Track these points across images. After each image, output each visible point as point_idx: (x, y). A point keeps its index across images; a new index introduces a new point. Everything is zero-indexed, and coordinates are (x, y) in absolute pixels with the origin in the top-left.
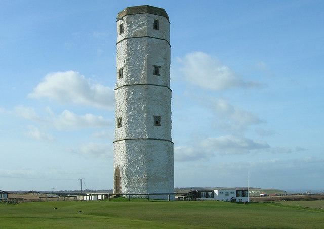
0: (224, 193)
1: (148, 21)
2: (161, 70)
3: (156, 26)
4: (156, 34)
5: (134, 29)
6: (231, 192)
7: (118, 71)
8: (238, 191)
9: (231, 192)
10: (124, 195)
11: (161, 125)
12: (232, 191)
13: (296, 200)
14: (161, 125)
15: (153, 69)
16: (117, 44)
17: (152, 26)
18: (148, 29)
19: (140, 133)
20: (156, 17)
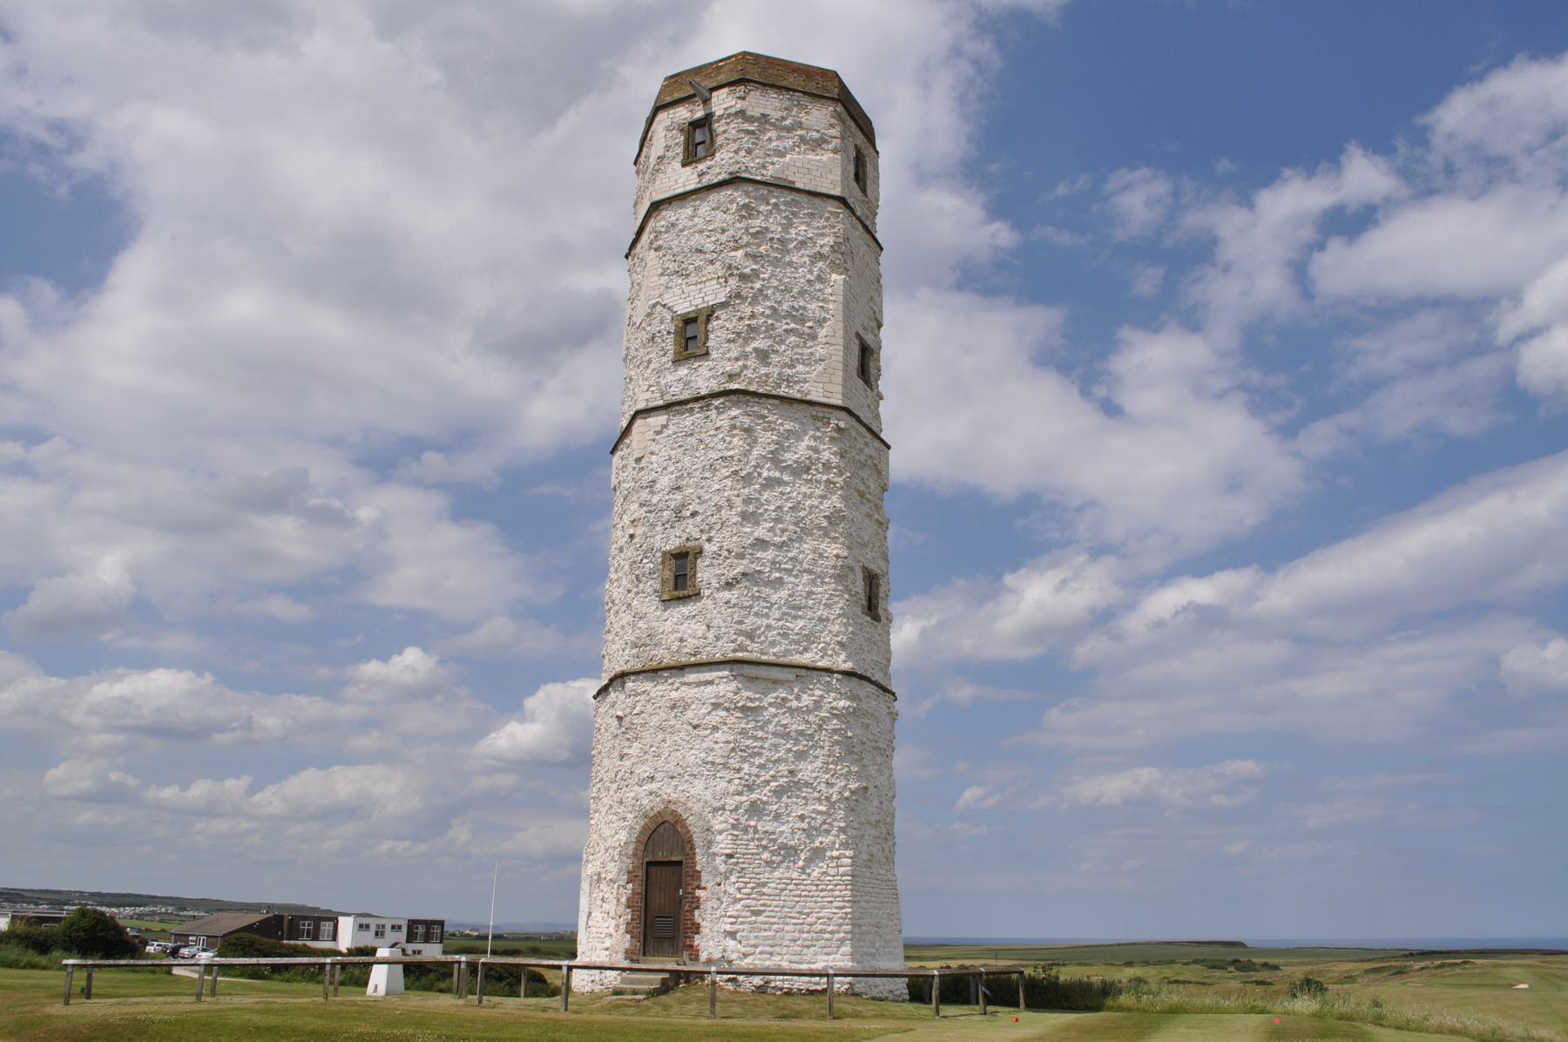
0: (373, 929)
6: (393, 927)
9: (393, 927)
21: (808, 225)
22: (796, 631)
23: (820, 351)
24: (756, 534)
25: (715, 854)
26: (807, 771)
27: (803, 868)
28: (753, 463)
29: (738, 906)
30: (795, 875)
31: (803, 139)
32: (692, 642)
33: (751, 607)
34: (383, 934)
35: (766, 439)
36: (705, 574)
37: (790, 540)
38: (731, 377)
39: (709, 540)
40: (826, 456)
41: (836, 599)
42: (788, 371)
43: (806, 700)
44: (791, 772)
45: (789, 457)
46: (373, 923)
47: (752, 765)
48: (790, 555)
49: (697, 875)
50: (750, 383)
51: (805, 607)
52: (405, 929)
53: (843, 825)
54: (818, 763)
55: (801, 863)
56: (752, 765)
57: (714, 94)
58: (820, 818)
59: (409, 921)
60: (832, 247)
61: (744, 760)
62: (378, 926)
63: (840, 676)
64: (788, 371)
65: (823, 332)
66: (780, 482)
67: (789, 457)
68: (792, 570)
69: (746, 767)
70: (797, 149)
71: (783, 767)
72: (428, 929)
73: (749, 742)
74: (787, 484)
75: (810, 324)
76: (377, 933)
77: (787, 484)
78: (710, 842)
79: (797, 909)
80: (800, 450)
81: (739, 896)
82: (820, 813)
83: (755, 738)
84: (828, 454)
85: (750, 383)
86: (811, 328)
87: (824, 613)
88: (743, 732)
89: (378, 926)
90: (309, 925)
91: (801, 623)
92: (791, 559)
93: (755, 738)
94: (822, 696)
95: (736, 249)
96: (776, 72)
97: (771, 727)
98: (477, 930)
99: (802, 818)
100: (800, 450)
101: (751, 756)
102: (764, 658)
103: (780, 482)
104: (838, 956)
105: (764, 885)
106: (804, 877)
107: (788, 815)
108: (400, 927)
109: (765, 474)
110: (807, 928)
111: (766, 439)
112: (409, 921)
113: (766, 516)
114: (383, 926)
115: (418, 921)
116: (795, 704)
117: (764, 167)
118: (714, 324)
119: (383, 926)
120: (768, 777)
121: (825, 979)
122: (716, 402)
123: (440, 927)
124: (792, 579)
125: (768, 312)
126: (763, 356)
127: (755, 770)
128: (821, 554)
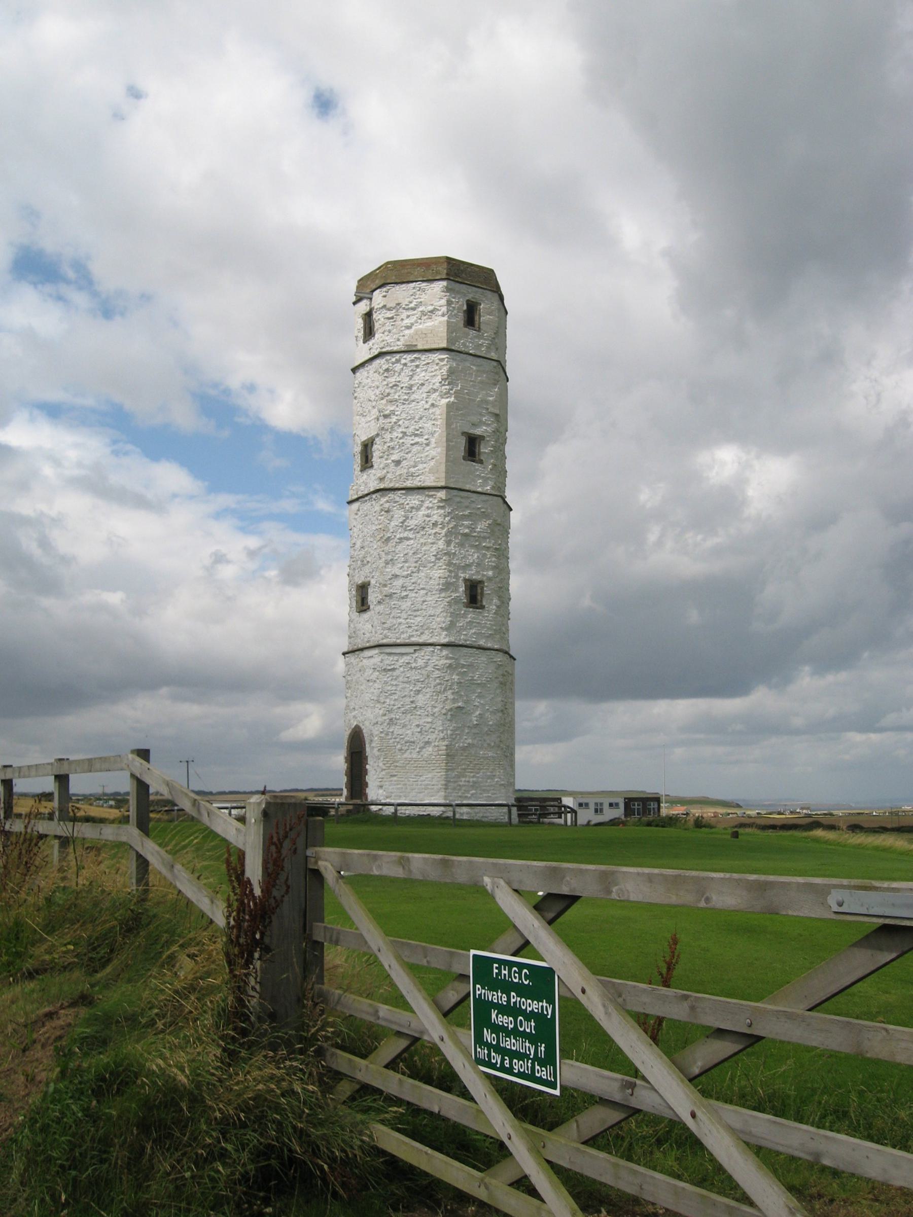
0: (592, 807)
1: (449, 303)
2: (485, 449)
3: (471, 316)
4: (469, 341)
5: (167, 987)
6: (611, 805)
7: (358, 449)
8: (629, 802)
9: (611, 805)
10: (374, 808)
11: (482, 607)
12: (613, 800)
13: (764, 828)
14: (482, 607)
15: (462, 442)
16: (354, 370)
17: (460, 318)
18: (450, 328)
19: (423, 628)
20: (472, 293)
21: (426, 371)
22: (416, 624)
23: (433, 453)
24: (393, 572)
25: (373, 747)
26: (421, 700)
27: (418, 752)
28: (391, 531)
29: (384, 773)
30: (414, 756)
31: (423, 313)
32: (368, 635)
33: (390, 614)
34: (601, 810)
35: (398, 514)
36: (372, 597)
37: (412, 572)
38: (382, 479)
39: (373, 577)
40: (435, 518)
41: (440, 603)
42: (412, 470)
43: (420, 663)
44: (412, 702)
45: (412, 523)
46: (592, 802)
47: (391, 699)
48: (412, 581)
49: (366, 758)
50: (391, 482)
51: (421, 610)
52: (622, 806)
53: (441, 728)
54: (428, 696)
55: (418, 750)
56: (391, 699)
57: (375, 293)
58: (428, 725)
59: (625, 799)
60: (440, 383)
61: (386, 697)
62: (596, 804)
63: (439, 647)
64: (412, 470)
65: (433, 440)
66: (408, 539)
67: (412, 523)
68: (413, 590)
69: (388, 700)
70: (419, 321)
71: (408, 700)
72: (644, 806)
73: (389, 688)
74: (411, 539)
75: (426, 437)
76: (596, 811)
77: (411, 539)
78: (371, 741)
79: (415, 773)
80: (418, 518)
81: (384, 768)
82: (428, 723)
83: (392, 685)
84: (437, 515)
85: (391, 482)
86: (427, 439)
87: (431, 612)
88: (386, 683)
89: (596, 804)
90: (638, 805)
91: (419, 619)
92: (413, 583)
93: (392, 685)
94: (429, 660)
95: (382, 399)
96: (406, 271)
97: (401, 679)
98: (808, 809)
99: (418, 726)
100: (418, 518)
101: (391, 695)
102: (398, 641)
103: (408, 539)
104: (437, 797)
105: (397, 762)
106: (419, 757)
107: (411, 725)
108: (617, 804)
109: (398, 536)
110: (419, 783)
111: (398, 514)
112: (625, 799)
113: (399, 561)
114: (601, 804)
115: (633, 798)
116: (413, 665)
117: (398, 340)
118: (375, 447)
119: (601, 804)
120: (399, 706)
121: (451, 808)
122: (374, 496)
123: (656, 804)
124: (414, 595)
125: (400, 435)
126: (398, 463)
127: (392, 702)
128: (431, 578)
